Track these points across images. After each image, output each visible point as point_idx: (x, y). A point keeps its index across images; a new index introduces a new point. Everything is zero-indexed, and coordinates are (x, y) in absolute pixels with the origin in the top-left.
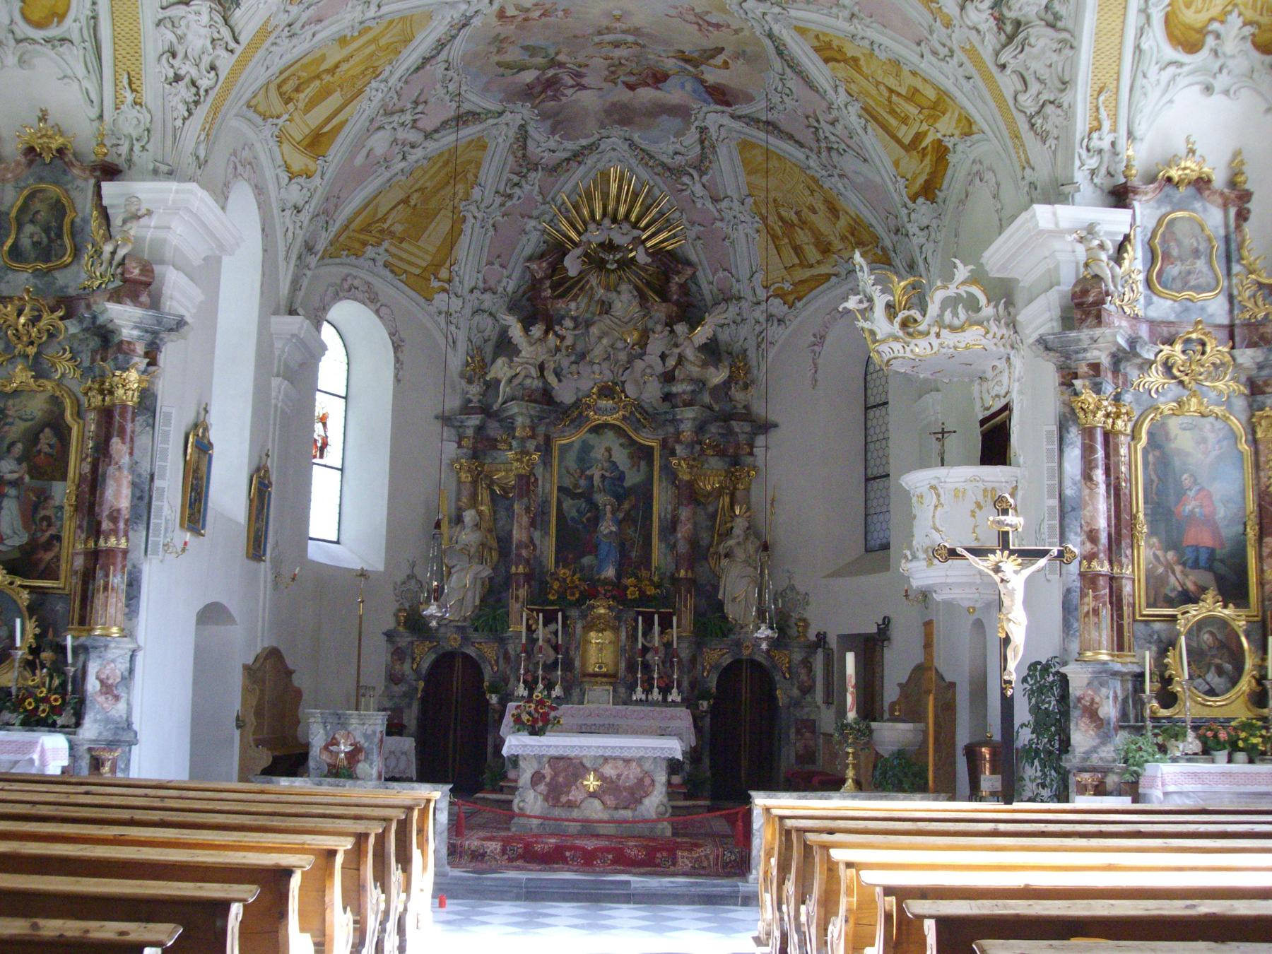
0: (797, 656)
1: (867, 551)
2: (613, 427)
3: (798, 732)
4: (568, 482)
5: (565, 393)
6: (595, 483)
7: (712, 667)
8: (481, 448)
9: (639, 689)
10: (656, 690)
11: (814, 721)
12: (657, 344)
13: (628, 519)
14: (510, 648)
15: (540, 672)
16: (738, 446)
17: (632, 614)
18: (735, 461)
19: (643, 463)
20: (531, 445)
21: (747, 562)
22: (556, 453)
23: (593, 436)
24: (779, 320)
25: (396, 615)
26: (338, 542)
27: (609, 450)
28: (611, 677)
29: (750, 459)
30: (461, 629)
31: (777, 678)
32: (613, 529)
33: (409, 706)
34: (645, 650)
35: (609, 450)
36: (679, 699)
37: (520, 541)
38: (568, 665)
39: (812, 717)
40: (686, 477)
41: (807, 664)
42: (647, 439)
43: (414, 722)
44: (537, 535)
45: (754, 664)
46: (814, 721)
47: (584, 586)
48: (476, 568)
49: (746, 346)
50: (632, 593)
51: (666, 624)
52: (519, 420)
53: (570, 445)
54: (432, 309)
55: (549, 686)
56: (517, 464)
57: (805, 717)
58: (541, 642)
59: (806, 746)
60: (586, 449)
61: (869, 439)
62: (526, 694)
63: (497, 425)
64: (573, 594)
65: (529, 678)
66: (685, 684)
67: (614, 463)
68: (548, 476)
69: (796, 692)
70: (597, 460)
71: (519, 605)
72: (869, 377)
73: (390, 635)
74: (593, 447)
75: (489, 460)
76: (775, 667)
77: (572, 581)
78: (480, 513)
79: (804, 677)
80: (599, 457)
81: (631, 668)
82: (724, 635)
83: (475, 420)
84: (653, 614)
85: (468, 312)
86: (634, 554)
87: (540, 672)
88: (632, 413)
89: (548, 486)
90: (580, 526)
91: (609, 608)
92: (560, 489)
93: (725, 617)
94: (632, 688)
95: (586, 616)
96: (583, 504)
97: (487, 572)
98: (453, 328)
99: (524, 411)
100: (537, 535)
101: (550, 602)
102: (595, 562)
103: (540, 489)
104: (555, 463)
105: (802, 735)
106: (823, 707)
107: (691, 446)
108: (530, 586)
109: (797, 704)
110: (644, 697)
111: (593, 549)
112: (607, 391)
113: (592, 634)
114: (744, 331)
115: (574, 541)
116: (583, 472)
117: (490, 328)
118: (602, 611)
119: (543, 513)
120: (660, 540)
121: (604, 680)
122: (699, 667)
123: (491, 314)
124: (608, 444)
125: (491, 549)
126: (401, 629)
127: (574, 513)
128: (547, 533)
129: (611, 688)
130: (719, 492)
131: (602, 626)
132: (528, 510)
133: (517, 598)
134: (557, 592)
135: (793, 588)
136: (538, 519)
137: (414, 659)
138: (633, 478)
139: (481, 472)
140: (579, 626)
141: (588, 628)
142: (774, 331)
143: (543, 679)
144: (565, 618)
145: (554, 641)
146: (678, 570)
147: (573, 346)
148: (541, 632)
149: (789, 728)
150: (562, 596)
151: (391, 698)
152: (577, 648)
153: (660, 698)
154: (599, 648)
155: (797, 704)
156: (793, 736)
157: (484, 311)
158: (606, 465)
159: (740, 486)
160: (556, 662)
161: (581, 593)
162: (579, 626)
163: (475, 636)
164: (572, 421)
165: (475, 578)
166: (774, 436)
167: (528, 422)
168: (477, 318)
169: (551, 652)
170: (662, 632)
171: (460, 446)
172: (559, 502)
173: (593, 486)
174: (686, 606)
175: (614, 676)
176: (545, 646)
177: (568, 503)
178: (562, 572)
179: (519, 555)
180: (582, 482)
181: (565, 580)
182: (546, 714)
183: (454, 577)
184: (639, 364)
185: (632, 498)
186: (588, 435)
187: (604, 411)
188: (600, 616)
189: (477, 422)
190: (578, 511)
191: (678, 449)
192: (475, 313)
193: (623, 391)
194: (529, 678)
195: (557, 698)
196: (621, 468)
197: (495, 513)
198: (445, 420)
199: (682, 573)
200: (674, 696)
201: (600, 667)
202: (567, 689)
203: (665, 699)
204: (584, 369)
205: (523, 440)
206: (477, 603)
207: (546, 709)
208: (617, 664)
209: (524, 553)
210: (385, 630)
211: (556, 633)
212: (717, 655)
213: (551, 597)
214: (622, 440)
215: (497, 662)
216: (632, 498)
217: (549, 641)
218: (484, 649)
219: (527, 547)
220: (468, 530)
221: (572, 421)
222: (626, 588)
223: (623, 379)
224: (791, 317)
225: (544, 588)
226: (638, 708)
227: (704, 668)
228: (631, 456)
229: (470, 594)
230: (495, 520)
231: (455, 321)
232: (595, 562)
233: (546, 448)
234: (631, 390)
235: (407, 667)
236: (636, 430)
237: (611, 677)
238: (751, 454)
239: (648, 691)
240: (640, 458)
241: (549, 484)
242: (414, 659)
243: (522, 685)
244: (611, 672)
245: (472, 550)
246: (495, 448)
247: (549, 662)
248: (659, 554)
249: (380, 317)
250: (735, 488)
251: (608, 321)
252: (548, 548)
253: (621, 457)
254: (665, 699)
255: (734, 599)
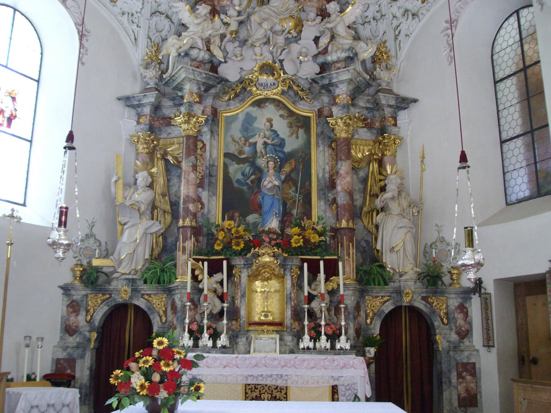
0: (454, 302)
1: (507, 204)
2: (274, 100)
3: (459, 376)
4: (233, 149)
5: (230, 72)
6: (258, 150)
7: (375, 314)
8: (158, 122)
9: (306, 337)
10: (323, 338)
11: (474, 364)
12: (309, 32)
13: (288, 180)
14: (177, 298)
15: (205, 321)
16: (384, 118)
17: (296, 261)
18: (382, 131)
19: (301, 132)
20: (198, 109)
21: (402, 215)
22: (222, 124)
23: (256, 108)
24: (413, 15)
25: (73, 270)
26: (24, 205)
27: (270, 121)
28: (278, 325)
29: (394, 130)
30: (132, 281)
31: (436, 324)
32: (277, 183)
33: (82, 357)
34: (311, 298)
35: (270, 121)
36: (348, 346)
37: (188, 196)
38: (234, 314)
39: (473, 360)
40: (344, 135)
41: (463, 309)
42: (304, 109)
43: (87, 373)
44: (204, 195)
45: (412, 310)
46: (474, 364)
47: (249, 236)
48: (146, 223)
49: (385, 38)
50: (296, 242)
51: (332, 270)
52: (187, 87)
53: (235, 117)
54: (116, 10)
55: (215, 336)
56: (185, 126)
57: (465, 361)
58: (206, 292)
59: (467, 391)
60: (249, 120)
61: (501, 107)
62: (191, 343)
63: (171, 103)
64: (238, 244)
65: (195, 327)
66: (351, 332)
67: (275, 132)
68: (215, 143)
69: (454, 337)
70: (260, 130)
71: (185, 257)
72: (495, 57)
73: (66, 289)
74: (256, 118)
75: (164, 135)
76: (434, 312)
77: (237, 232)
78: (151, 175)
79: (460, 322)
80: (262, 127)
81: (297, 315)
82: (386, 284)
83: (151, 98)
84: (318, 261)
85: (147, 12)
86: (294, 212)
87: (205, 321)
88: (290, 88)
89: (215, 152)
90: (245, 188)
91: (275, 256)
92: (226, 155)
93: (383, 267)
94: (299, 336)
95: (252, 264)
96: (247, 169)
97: (157, 227)
98: (134, 27)
99: (192, 77)
100: (204, 195)
101: (217, 256)
102: (259, 220)
103: (208, 154)
104: (222, 132)
105: (463, 378)
106: (483, 351)
107: (346, 107)
108: (197, 241)
109: (456, 348)
110: (311, 345)
111: (258, 208)
112: (267, 69)
113: (258, 283)
114: (382, 26)
115: (238, 201)
116: (246, 140)
117: (167, 28)
118: (267, 259)
119: (210, 175)
120: (319, 198)
121: (271, 328)
122: (362, 314)
123: (167, 17)
124: (269, 116)
125: (165, 212)
126: (77, 282)
127: (239, 176)
128: (215, 194)
129: (278, 337)
130: (370, 159)
131: (267, 275)
132: (194, 167)
133: (184, 248)
134: (222, 241)
135: (442, 240)
136: (206, 180)
137: (88, 311)
138: (292, 144)
139: (157, 146)
140: (244, 275)
141: (253, 277)
142: (406, 25)
143: (208, 328)
144: (230, 268)
145: (219, 291)
146: (338, 219)
147: (237, 32)
148: (206, 283)
149: (450, 371)
150: (227, 246)
151: (65, 348)
152: (243, 296)
153: (328, 345)
154: (265, 298)
155: (456, 348)
156: (454, 379)
157: (161, 13)
158: (268, 133)
159: (388, 153)
160: (221, 314)
161: (246, 243)
162: (244, 275)
163: (145, 288)
164: (237, 95)
165: (145, 233)
166: (414, 109)
167: (195, 89)
168: (155, 19)
169: (217, 301)
170: (327, 280)
171: (138, 123)
172: (226, 167)
173: (256, 152)
174: (349, 255)
175: (280, 324)
176: (211, 295)
177: (233, 168)
178: (227, 223)
179: (186, 210)
180: (247, 149)
181: (230, 230)
182: (175, 375)
183: (126, 233)
184: (295, 48)
185: (293, 161)
186: (251, 108)
187: (265, 86)
188: (265, 265)
189: (153, 100)
190: (243, 174)
191: (335, 110)
192: (153, 14)
193: (282, 68)
194: (195, 327)
195: (224, 347)
196: (282, 135)
197: (169, 180)
198: (127, 101)
199: (344, 224)
200: (343, 343)
201: (266, 316)
202: (233, 338)
203: (333, 347)
204: (248, 53)
205: (190, 104)
206: (147, 256)
207: (175, 367)
208: (282, 313)
209: (191, 207)
210: (62, 284)
211: (221, 283)
212: (379, 303)
213: (217, 248)
214: (282, 112)
215: (165, 312)
216: (293, 161)
217: (215, 291)
218: (153, 301)
219: (194, 201)
220: (140, 190)
221: (237, 95)
222: (291, 237)
223: (281, 58)
224: (424, 11)
225: (212, 238)
226: (306, 356)
227: (367, 315)
228: (290, 126)
229: (140, 249)
230: (168, 187)
231: (136, 21)
232: (259, 220)
233: (214, 117)
234: (287, 66)
235: (81, 320)
236: (294, 103)
237: (278, 325)
238: (395, 125)
239: (315, 338)
240: (298, 127)
241: (215, 149)
242: (88, 311)
243: (186, 335)
244: (277, 320)
245: (143, 208)
246: (169, 124)
247: (215, 311)
248: (318, 207)
249: (66, 7)
250: (383, 155)
251: (267, 10)
252: (215, 207)
253: (281, 126)
254: (333, 347)
255: (392, 249)
